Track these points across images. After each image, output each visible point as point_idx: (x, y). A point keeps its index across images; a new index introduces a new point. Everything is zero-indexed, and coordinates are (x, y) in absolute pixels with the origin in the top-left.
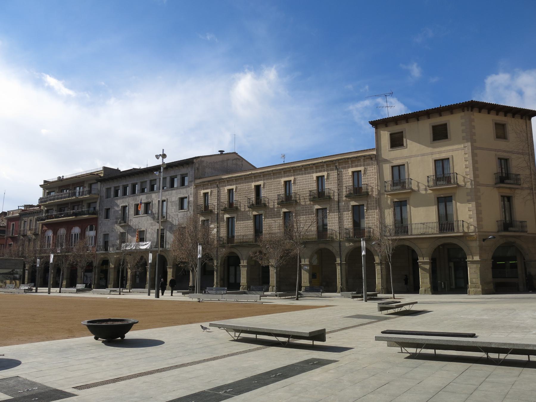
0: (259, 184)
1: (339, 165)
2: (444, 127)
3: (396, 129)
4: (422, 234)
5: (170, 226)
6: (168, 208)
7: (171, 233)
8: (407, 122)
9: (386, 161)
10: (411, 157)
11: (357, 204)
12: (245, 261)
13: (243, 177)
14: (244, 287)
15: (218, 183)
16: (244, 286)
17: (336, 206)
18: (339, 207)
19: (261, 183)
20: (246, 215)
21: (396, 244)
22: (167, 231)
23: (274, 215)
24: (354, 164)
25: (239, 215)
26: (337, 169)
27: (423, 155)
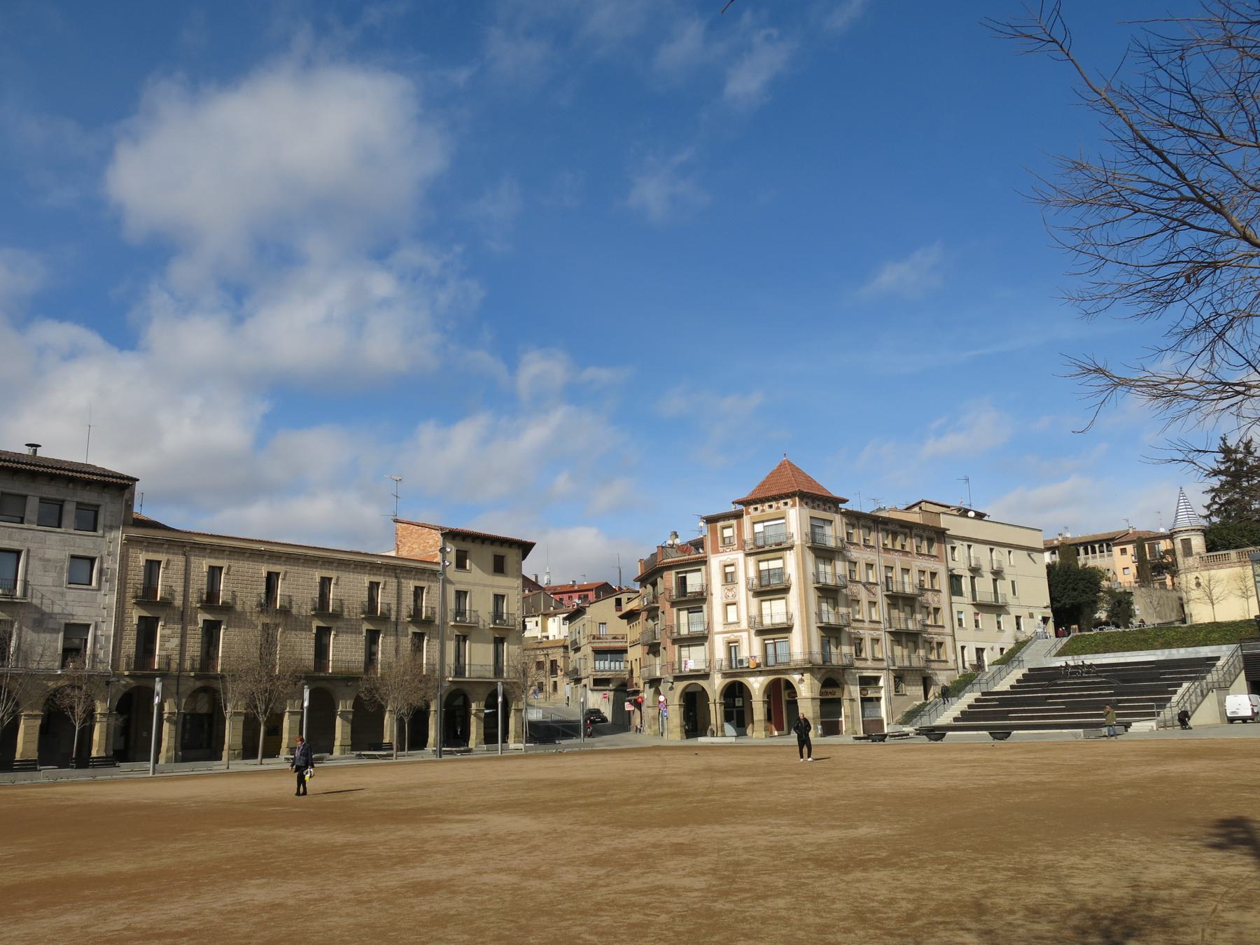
1: (400, 573)
2: (95, 509)
3: (465, 546)
4: (479, 678)
5: (36, 616)
6: (29, 572)
8: (473, 542)
9: (451, 582)
10: (475, 584)
11: (149, 615)
12: (350, 703)
13: (208, 547)
14: (236, 752)
15: (188, 548)
16: (234, 750)
19: (162, 557)
21: (454, 687)
23: (299, 624)
24: (387, 574)
26: (396, 577)
27: (485, 586)
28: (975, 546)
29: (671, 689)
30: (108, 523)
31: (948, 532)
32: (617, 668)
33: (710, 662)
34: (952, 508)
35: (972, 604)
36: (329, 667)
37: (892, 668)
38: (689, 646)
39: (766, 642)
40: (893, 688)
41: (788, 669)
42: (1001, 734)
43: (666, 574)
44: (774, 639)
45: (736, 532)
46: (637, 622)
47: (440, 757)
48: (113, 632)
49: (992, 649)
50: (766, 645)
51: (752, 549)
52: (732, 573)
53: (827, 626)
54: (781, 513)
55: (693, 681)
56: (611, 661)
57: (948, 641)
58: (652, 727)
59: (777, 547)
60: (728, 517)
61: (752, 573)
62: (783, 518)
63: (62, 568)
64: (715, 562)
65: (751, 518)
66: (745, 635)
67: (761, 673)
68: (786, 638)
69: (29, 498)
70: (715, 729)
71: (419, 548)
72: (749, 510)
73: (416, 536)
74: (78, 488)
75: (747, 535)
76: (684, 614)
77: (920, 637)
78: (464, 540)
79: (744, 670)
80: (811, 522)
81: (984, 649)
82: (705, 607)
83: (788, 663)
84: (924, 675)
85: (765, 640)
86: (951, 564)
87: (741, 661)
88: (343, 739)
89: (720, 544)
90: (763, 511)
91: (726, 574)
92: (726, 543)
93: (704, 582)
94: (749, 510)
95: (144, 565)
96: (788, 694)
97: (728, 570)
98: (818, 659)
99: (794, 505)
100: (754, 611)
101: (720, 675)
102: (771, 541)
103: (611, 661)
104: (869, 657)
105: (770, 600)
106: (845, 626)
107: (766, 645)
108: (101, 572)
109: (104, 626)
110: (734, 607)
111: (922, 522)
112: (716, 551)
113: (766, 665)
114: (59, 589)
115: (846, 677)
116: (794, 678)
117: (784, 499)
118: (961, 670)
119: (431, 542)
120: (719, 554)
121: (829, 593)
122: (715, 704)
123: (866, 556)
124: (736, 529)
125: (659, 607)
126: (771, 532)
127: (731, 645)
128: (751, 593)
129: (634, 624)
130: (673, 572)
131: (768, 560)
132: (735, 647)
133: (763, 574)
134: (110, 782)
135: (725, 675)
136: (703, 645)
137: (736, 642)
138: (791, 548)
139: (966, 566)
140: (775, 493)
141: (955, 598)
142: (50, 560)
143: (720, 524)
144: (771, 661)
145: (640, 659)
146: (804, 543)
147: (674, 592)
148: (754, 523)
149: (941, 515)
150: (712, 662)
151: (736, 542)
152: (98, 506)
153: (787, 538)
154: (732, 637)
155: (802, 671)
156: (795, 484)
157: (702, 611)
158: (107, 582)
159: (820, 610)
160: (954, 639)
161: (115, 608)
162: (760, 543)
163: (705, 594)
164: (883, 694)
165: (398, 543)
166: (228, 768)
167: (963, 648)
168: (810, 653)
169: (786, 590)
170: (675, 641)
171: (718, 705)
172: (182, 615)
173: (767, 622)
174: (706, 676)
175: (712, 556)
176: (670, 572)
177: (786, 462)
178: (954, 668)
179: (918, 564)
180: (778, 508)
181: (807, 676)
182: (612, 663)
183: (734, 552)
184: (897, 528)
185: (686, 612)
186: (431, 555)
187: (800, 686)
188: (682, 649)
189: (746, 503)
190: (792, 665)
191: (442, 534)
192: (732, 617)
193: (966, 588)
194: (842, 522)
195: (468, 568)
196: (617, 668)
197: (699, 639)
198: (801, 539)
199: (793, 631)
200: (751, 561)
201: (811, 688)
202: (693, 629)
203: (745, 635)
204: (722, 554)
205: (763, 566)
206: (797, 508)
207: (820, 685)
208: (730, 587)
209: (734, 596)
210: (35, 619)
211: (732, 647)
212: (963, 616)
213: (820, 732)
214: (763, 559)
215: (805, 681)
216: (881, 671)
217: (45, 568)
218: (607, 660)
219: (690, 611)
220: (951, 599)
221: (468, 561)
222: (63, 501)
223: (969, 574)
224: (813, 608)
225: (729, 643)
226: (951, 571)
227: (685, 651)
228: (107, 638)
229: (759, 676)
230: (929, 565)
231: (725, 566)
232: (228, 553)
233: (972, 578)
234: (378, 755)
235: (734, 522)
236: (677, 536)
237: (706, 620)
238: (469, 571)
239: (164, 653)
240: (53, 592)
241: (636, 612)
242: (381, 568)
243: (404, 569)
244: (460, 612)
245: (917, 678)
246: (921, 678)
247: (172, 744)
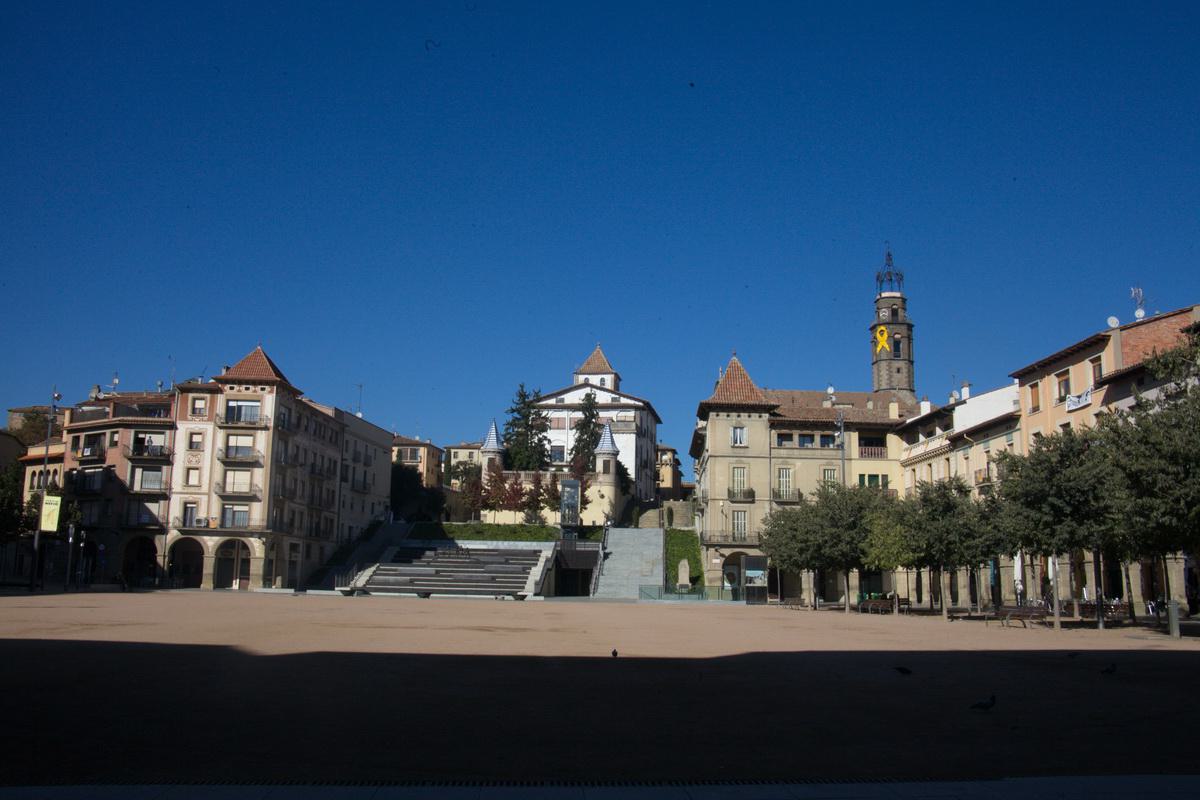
61: (220, 444)
62: (259, 401)
64: (183, 429)
82: (165, 468)
87: (199, 521)
90: (239, 391)
99: (271, 392)
110: (197, 472)
112: (184, 418)
132: (192, 508)
137: (194, 503)
143: (191, 396)
144: (228, 524)
154: (190, 498)
180: (255, 391)
203: (205, 498)
211: (187, 510)
235: (208, 396)
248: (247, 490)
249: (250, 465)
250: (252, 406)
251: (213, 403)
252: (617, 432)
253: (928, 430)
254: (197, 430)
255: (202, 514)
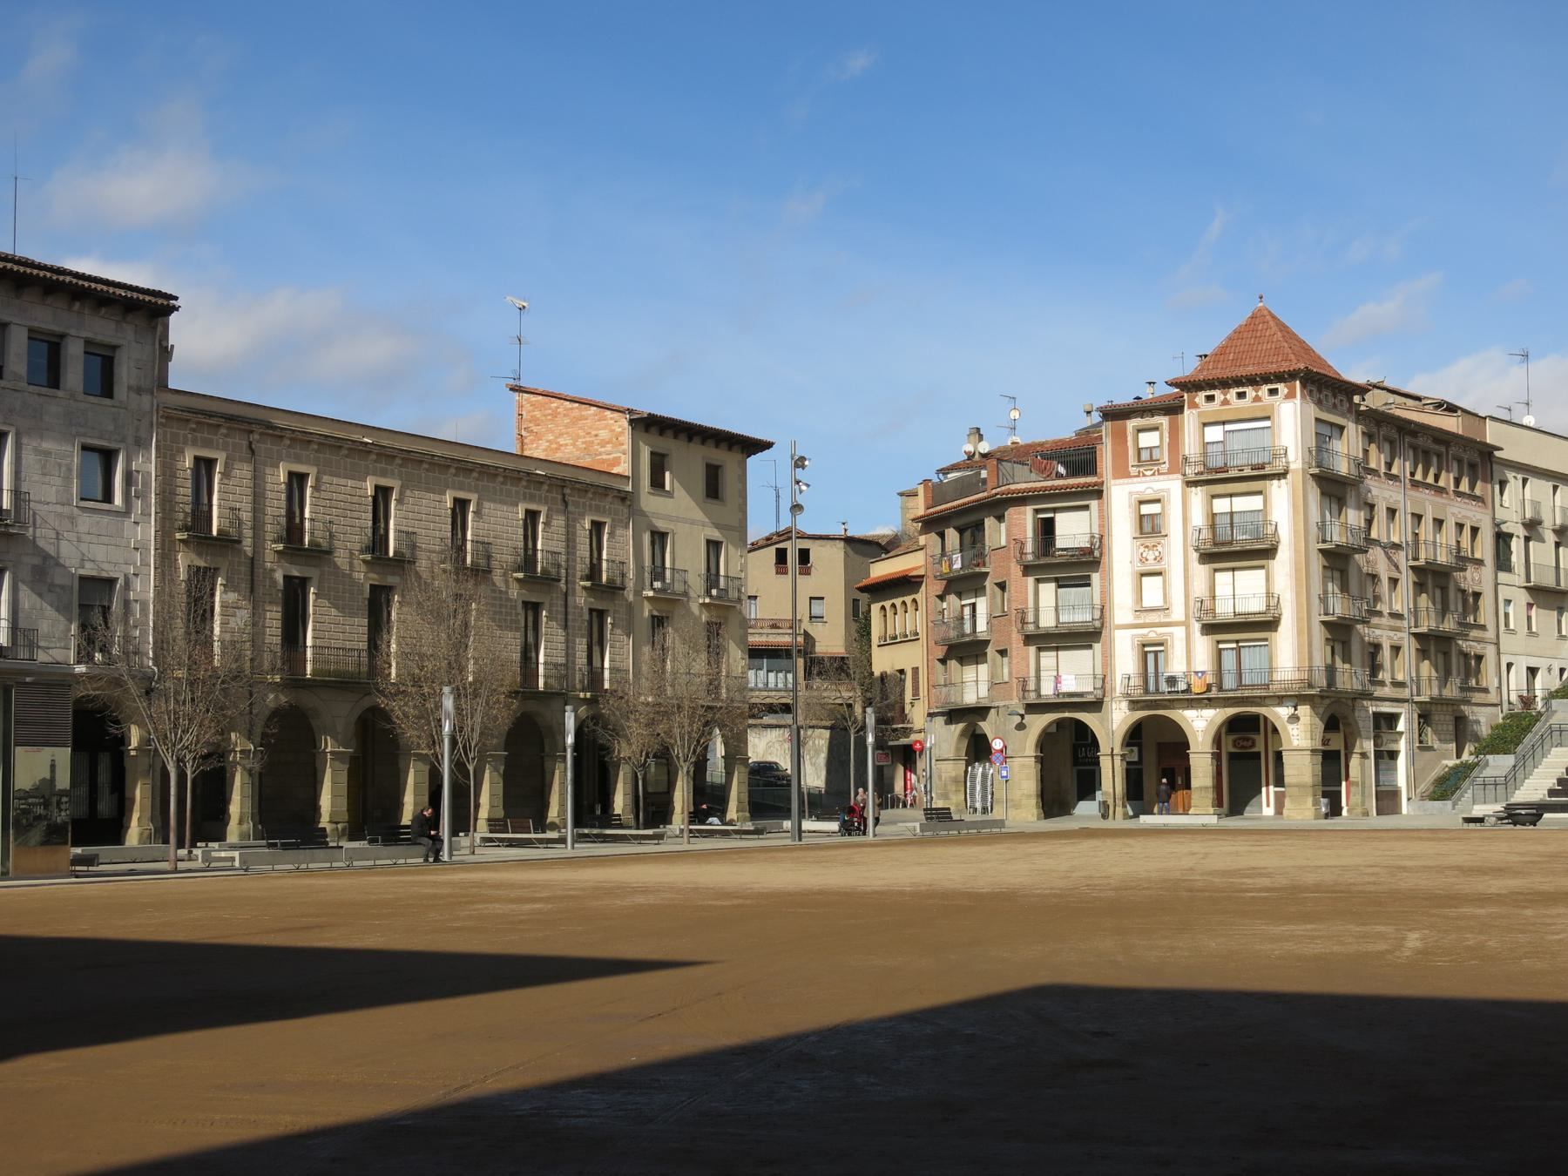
0: (390, 485)
3: (667, 444)
5: (36, 561)
7: (40, 595)
10: (678, 520)
13: (288, 434)
14: (340, 826)
15: (257, 437)
17: (561, 602)
18: (566, 606)
20: (503, 596)
22: (21, 585)
25: (326, 577)
28: (1533, 482)
29: (1021, 727)
30: (133, 382)
31: (1497, 454)
32: (780, 685)
33: (1104, 680)
34: (1424, 402)
35: (1525, 588)
36: (603, 680)
37: (1417, 699)
38: (1057, 649)
39: (1221, 646)
40: (1416, 736)
41: (1265, 697)
42: (1515, 825)
43: (1011, 513)
44: (1237, 642)
45: (1166, 440)
46: (908, 599)
47: (800, 840)
48: (152, 595)
49: (1549, 670)
50: (1220, 651)
51: (1202, 473)
52: (1152, 516)
53: (1340, 622)
54: (1263, 408)
55: (1067, 715)
56: (768, 671)
57: (1490, 652)
58: (951, 796)
59: (1255, 473)
60: (1150, 411)
61: (1198, 518)
62: (1268, 418)
63: (70, 470)
64: (1121, 495)
65: (1200, 414)
66: (1179, 632)
67: (1210, 703)
68: (1266, 640)
69: (13, 327)
70: (1110, 802)
71: (574, 445)
72: (1197, 400)
73: (567, 421)
74: (86, 311)
75: (1190, 447)
76: (1048, 591)
77: (1454, 644)
78: (662, 433)
79: (1181, 696)
80: (1316, 428)
81: (1538, 669)
82: (1095, 578)
83: (1267, 686)
84: (1458, 715)
85: (1218, 642)
86: (1500, 514)
87: (1172, 681)
88: (492, 806)
89: (1132, 460)
90: (1225, 402)
91: (1141, 517)
92: (1148, 461)
93: (1096, 530)
94: (1197, 400)
95: (192, 466)
96: (1234, 741)
97: (1145, 509)
98: (1321, 681)
99: (1290, 396)
100: (1199, 588)
101: (1124, 705)
102: (1240, 460)
103: (768, 671)
104: (1388, 680)
105: (1233, 569)
106: (1358, 622)
107: (1220, 651)
108: (129, 479)
109: (137, 584)
110: (1159, 579)
111: (1460, 433)
112: (1122, 472)
113: (1220, 689)
114: (66, 509)
115: (1356, 714)
116: (1282, 713)
117: (1271, 382)
118: (1505, 706)
119: (604, 434)
120: (1130, 480)
121: (1338, 561)
122: (1112, 755)
123: (1387, 494)
124: (1166, 435)
125: (987, 573)
126: (1236, 444)
127: (1147, 649)
128: (1195, 556)
129: (898, 601)
130: (1028, 511)
131: (1231, 495)
132: (1156, 653)
133: (1218, 520)
134: (556, 864)
135: (1135, 704)
136: (1090, 647)
137: (1161, 644)
138: (1282, 475)
139: (1516, 518)
140: (1251, 370)
141: (1503, 576)
142: (50, 453)
143: (1132, 424)
144: (1229, 682)
145: (915, 670)
146: (1306, 467)
147: (1029, 548)
148: (1205, 425)
149: (1487, 420)
150: (1108, 679)
151: (1166, 459)
152: (114, 348)
153: (1275, 456)
154: (1152, 634)
155: (1299, 699)
156: (1292, 357)
157: (1089, 585)
158: (137, 497)
159: (1325, 592)
160: (1498, 649)
161: (152, 548)
162: (1218, 462)
163: (1097, 554)
164: (1402, 745)
165: (523, 433)
166: (473, 853)
167: (1509, 665)
168: (1311, 669)
169: (1269, 553)
170: (1029, 639)
171: (1118, 760)
172: (252, 564)
173: (1224, 610)
174: (1096, 706)
175: (1113, 482)
176: (1022, 508)
177: (1265, 313)
178: (1495, 702)
179: (1455, 510)
180: (1257, 399)
181: (1304, 711)
182: (772, 675)
183: (1162, 477)
184: (1429, 444)
185: (1053, 585)
186: (604, 461)
187: (1290, 727)
188: (1042, 654)
189: (1190, 385)
190: (1275, 689)
191: (631, 422)
192: (1153, 596)
193: (1518, 557)
194: (1357, 432)
195: (667, 487)
196: (780, 685)
197: (1084, 637)
198: (1303, 459)
199: (1279, 629)
200: (1198, 495)
201: (1311, 731)
202: (1065, 618)
203: (1179, 632)
204: (1135, 480)
205: (1221, 506)
206: (1298, 400)
207: (1323, 727)
208: (1150, 542)
209: (1158, 559)
210: (34, 567)
211: (1150, 652)
212: (1511, 610)
213: (1324, 809)
214: (1223, 492)
215: (1302, 718)
216: (1401, 705)
217: (44, 467)
218: (761, 669)
219: (1061, 584)
220: (1496, 578)
221: (667, 475)
222: (63, 336)
223: (1521, 532)
224: (1317, 589)
225: (1144, 646)
226: (1498, 525)
227: (1048, 659)
228: (144, 606)
229: (1206, 707)
230: (1470, 514)
231: (1141, 502)
232: (316, 447)
233: (1527, 539)
234: (630, 835)
235: (1163, 421)
236: (981, 438)
237: (1097, 601)
238: (670, 494)
239: (228, 637)
240: (60, 515)
241: (913, 580)
242: (542, 483)
243: (577, 486)
244: (712, 578)
245: (1448, 718)
246: (1452, 718)
247: (248, 810)
248: (1263, 608)
249: (1262, 554)
250: (150, 575)
251: (1175, 433)
252: (17, 655)
253: (998, 513)
254: (1149, 495)
255: (1176, 665)
